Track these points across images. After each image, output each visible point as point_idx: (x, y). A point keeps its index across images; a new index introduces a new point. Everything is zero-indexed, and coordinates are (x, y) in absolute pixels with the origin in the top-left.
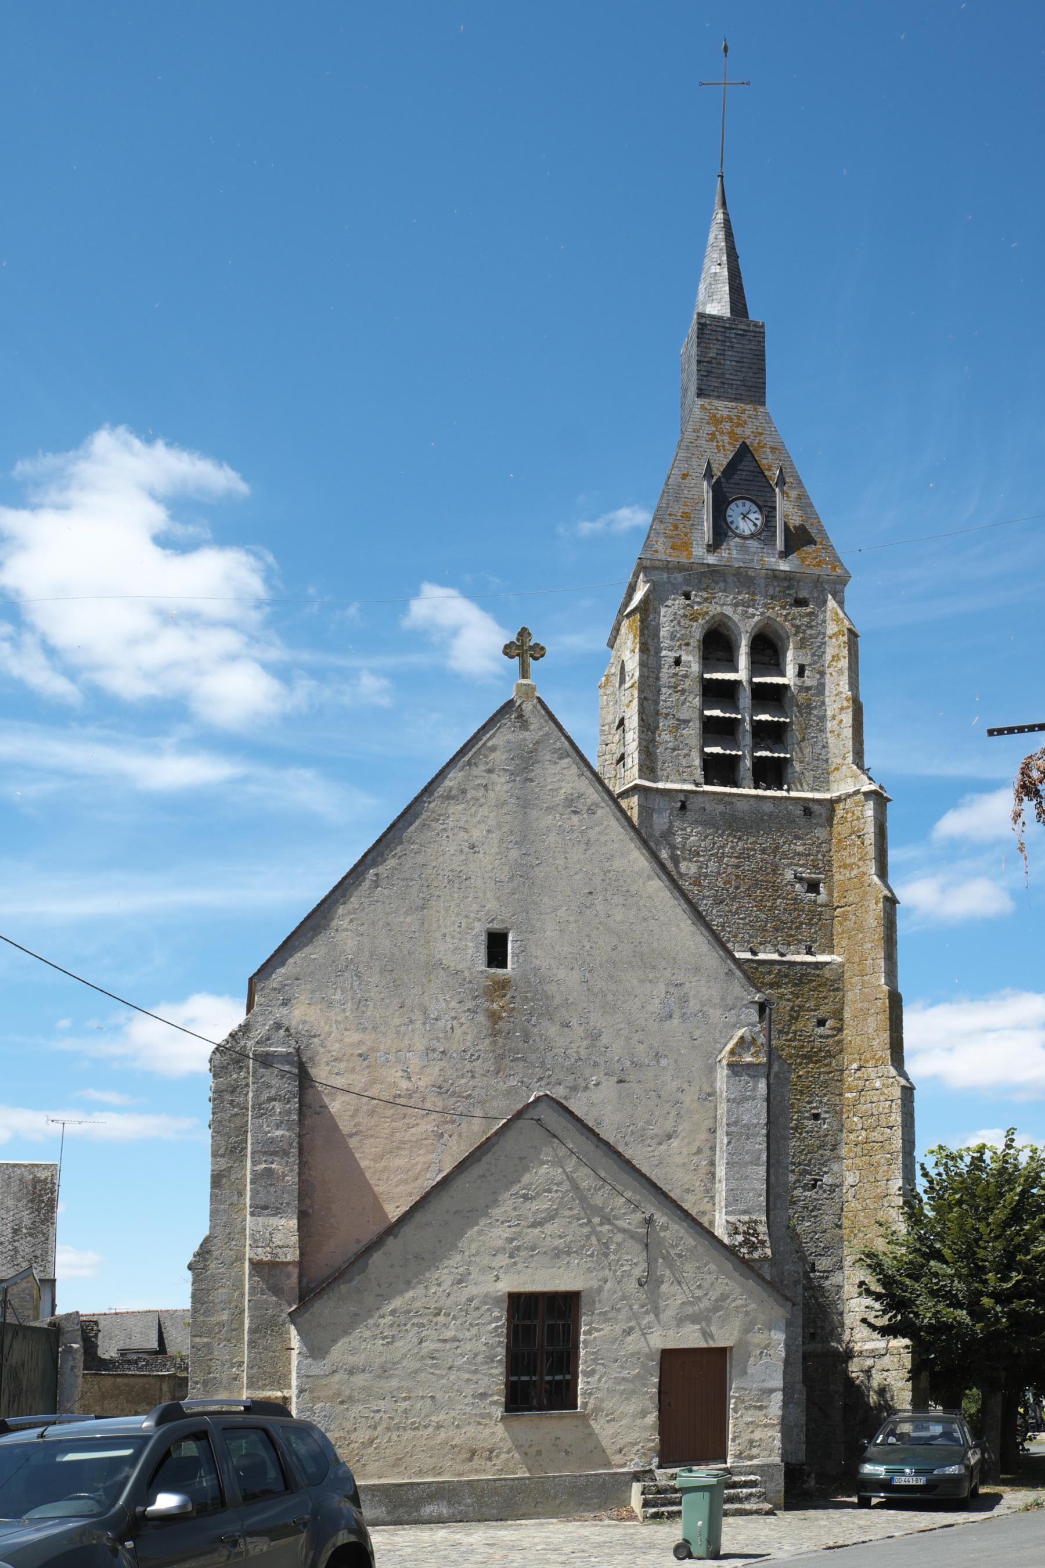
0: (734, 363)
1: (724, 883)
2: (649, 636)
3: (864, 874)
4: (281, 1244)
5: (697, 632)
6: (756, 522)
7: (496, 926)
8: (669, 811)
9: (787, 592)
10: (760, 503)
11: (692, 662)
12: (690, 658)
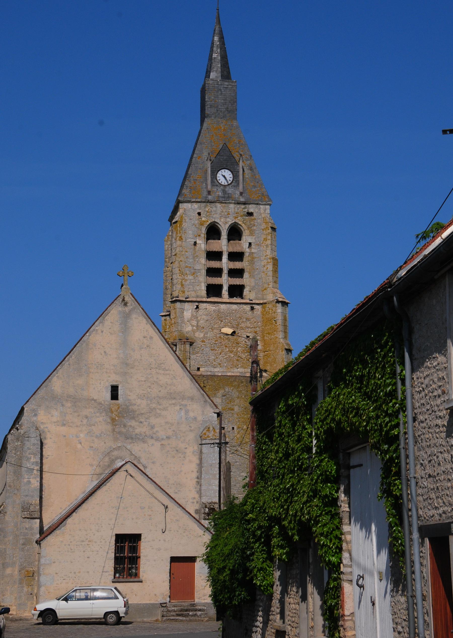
0: (222, 101)
1: (215, 341)
2: (182, 233)
3: (277, 337)
4: (32, 510)
5: (204, 230)
6: (229, 181)
7: (115, 384)
8: (191, 310)
9: (244, 210)
10: (232, 171)
11: (202, 244)
12: (201, 242)
